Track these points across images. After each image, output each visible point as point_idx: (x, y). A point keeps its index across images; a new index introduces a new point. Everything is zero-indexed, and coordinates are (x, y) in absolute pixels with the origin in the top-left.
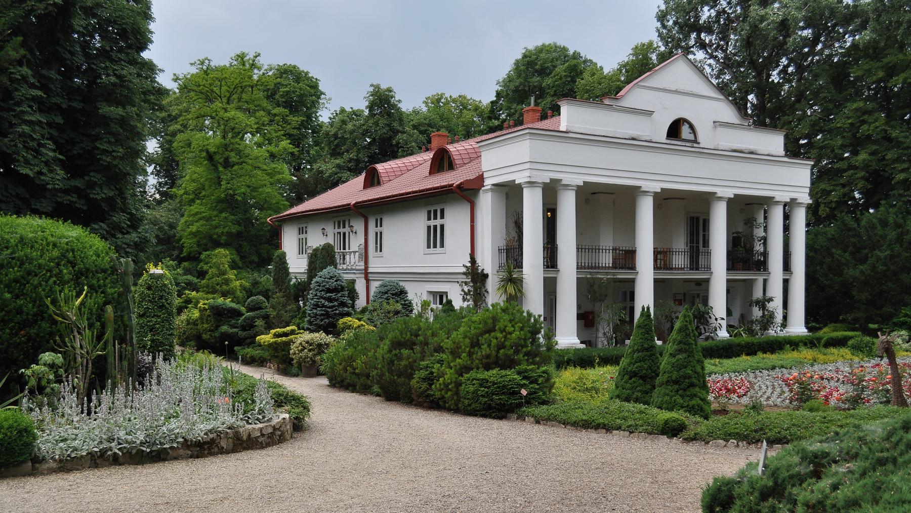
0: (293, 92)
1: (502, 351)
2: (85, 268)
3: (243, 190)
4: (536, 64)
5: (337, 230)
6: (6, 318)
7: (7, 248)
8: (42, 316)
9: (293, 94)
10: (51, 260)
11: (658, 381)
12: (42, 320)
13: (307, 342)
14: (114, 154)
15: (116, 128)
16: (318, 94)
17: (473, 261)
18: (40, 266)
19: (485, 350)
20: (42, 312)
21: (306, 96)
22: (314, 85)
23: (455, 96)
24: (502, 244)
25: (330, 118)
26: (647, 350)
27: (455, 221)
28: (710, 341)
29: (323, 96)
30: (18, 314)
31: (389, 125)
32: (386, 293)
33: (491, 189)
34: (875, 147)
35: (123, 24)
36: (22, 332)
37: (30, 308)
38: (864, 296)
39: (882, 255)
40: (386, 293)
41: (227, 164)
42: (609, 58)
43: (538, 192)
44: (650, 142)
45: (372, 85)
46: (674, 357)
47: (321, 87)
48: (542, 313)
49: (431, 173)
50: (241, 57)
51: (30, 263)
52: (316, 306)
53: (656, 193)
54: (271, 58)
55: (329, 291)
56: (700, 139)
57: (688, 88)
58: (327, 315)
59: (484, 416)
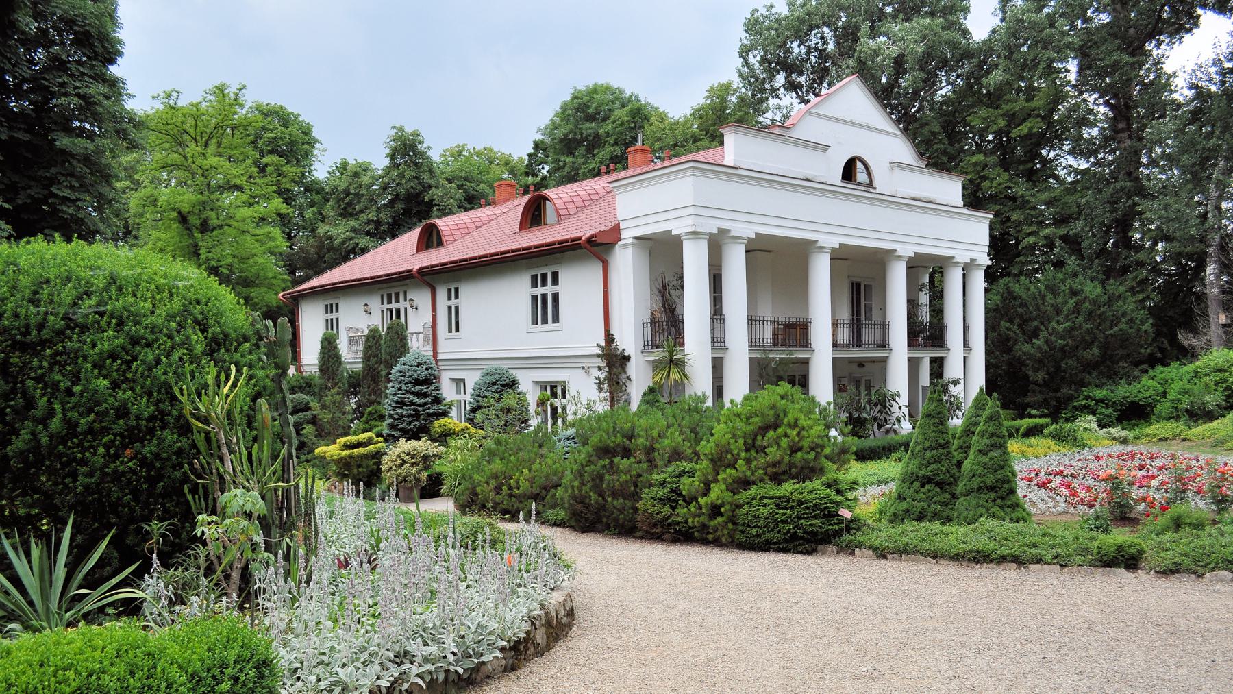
0: (282, 139)
1: (799, 455)
2: (222, 332)
3: (229, 260)
4: (589, 107)
6: (97, 426)
7: (88, 294)
8: (161, 420)
9: (282, 142)
10: (170, 317)
11: (960, 487)
12: (163, 428)
13: (408, 454)
14: (79, 203)
15: (80, 168)
16: (312, 143)
17: (609, 338)
19: (773, 454)
20: (163, 413)
21: (297, 143)
22: (307, 132)
23: (479, 148)
24: (647, 316)
26: (942, 446)
27: (577, 287)
28: (892, 436)
30: (119, 417)
31: (416, 178)
32: (494, 384)
34: (998, 207)
35: (86, 25)
36: (128, 452)
37: (143, 407)
38: (1041, 376)
40: (494, 384)
41: (205, 227)
42: (678, 103)
43: (703, 246)
45: (394, 127)
46: (985, 454)
48: (831, 400)
49: (520, 229)
50: (220, 90)
51: (135, 323)
52: (401, 404)
53: (833, 250)
54: (260, 92)
55: (418, 382)
56: (876, 183)
58: (417, 416)
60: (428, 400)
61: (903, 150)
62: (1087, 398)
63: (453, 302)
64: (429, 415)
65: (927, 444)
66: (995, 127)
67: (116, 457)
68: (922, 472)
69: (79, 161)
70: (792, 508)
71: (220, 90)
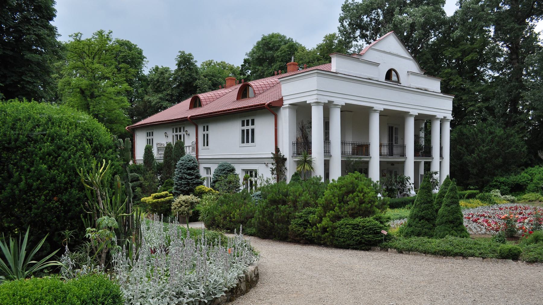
0: (128, 56)
1: (363, 205)
2: (99, 144)
3: (103, 111)
4: (270, 44)
5: (175, 134)
6: (41, 186)
7: (38, 126)
8: (71, 184)
9: (128, 57)
10: (76, 137)
11: (437, 221)
12: (71, 188)
13: (184, 201)
14: (35, 84)
16: (142, 58)
17: (277, 150)
18: (68, 142)
19: (352, 204)
20: (72, 181)
21: (136, 58)
22: (140, 53)
23: (219, 62)
24: (295, 140)
25: (150, 72)
26: (429, 202)
27: (263, 127)
28: (406, 197)
29: (144, 59)
32: (224, 170)
33: (289, 107)
36: (55, 198)
37: (62, 178)
38: (475, 171)
39: (484, 149)
40: (224, 170)
41: (92, 96)
42: (311, 43)
43: (321, 108)
44: (378, 81)
45: (180, 52)
46: (449, 206)
47: (144, 54)
49: (237, 99)
50: (100, 33)
52: (181, 178)
54: (119, 34)
55: (189, 169)
56: (401, 81)
57: (390, 52)
58: (188, 184)
59: (356, 249)
60: (194, 177)
61: (412, 66)
62: (496, 181)
63: (206, 132)
64: (194, 184)
65: (422, 201)
67: (50, 200)
68: (420, 214)
69: (35, 65)
70: (360, 229)
71: (100, 33)
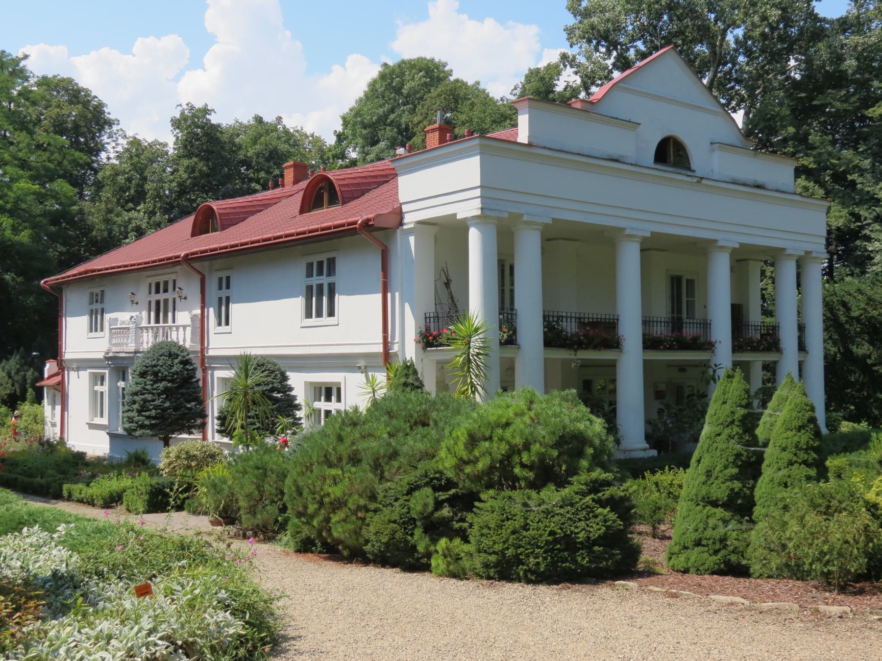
66: (608, 85)
